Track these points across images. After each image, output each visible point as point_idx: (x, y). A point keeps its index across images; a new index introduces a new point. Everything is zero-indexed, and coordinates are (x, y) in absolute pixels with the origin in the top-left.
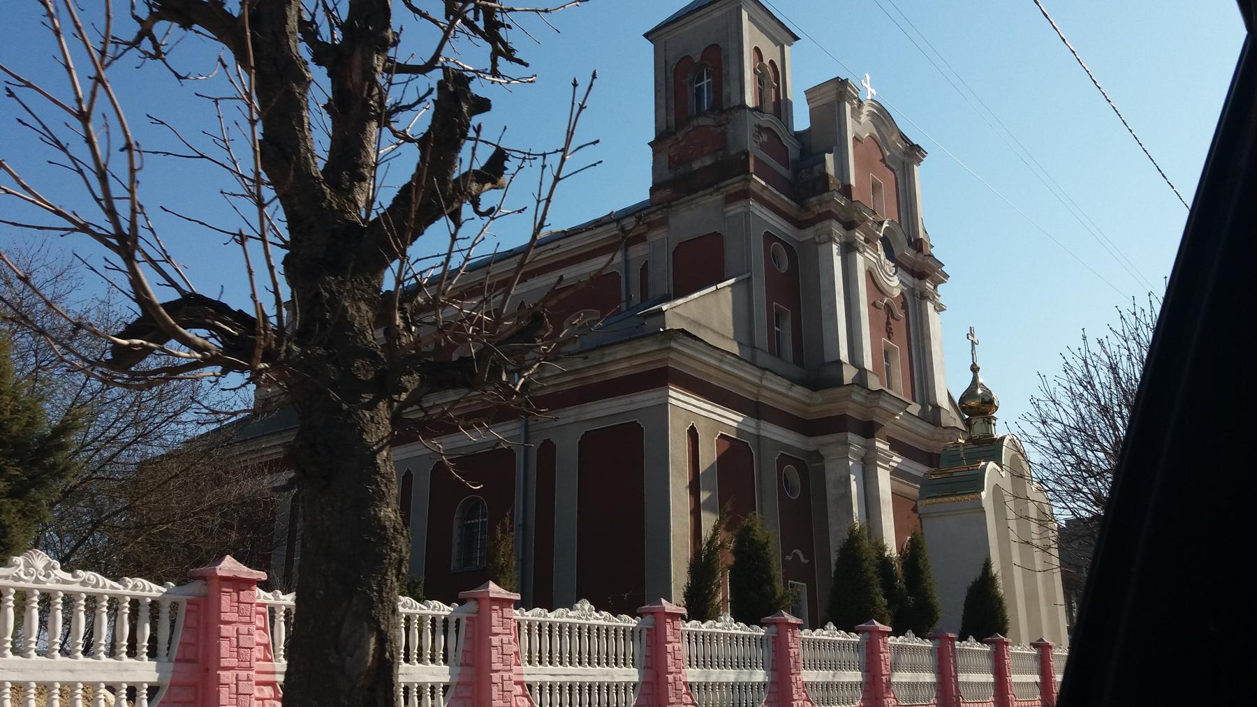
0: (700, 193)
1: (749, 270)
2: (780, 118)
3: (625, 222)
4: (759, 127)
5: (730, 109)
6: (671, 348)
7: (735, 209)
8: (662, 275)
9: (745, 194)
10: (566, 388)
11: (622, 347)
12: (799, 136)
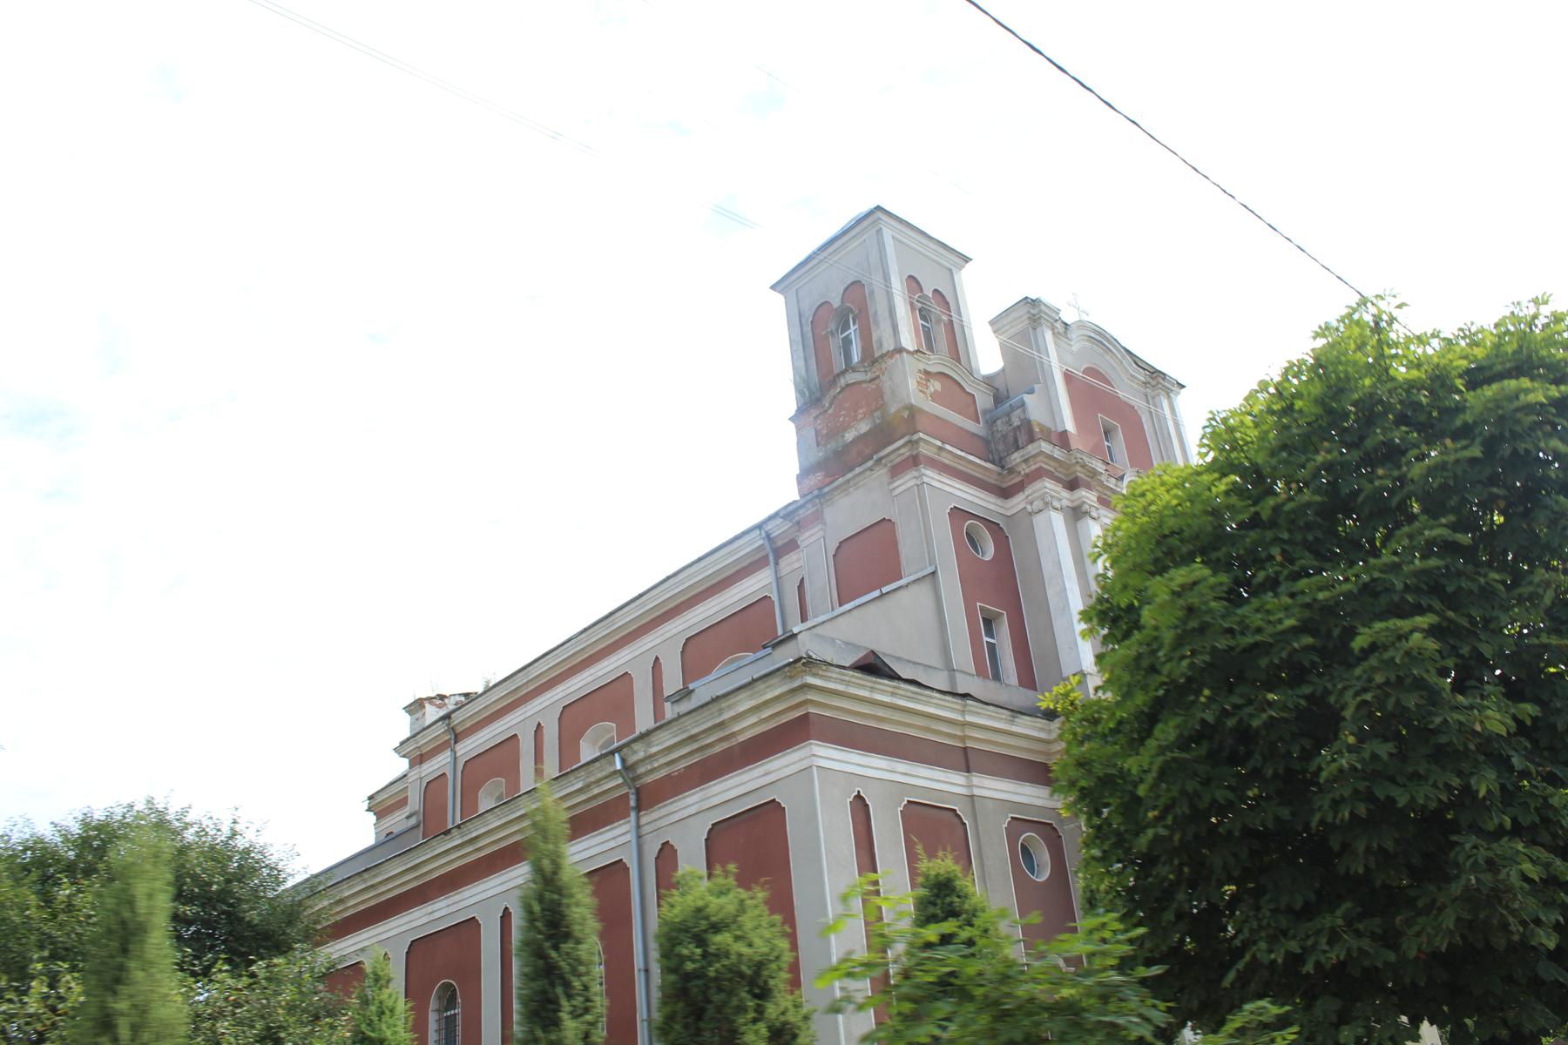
0: (858, 470)
1: (932, 561)
2: (958, 360)
3: (768, 527)
4: (927, 373)
5: (882, 356)
6: (806, 687)
7: (907, 481)
8: (822, 584)
9: (915, 461)
10: (682, 765)
11: (742, 695)
12: (989, 381)
